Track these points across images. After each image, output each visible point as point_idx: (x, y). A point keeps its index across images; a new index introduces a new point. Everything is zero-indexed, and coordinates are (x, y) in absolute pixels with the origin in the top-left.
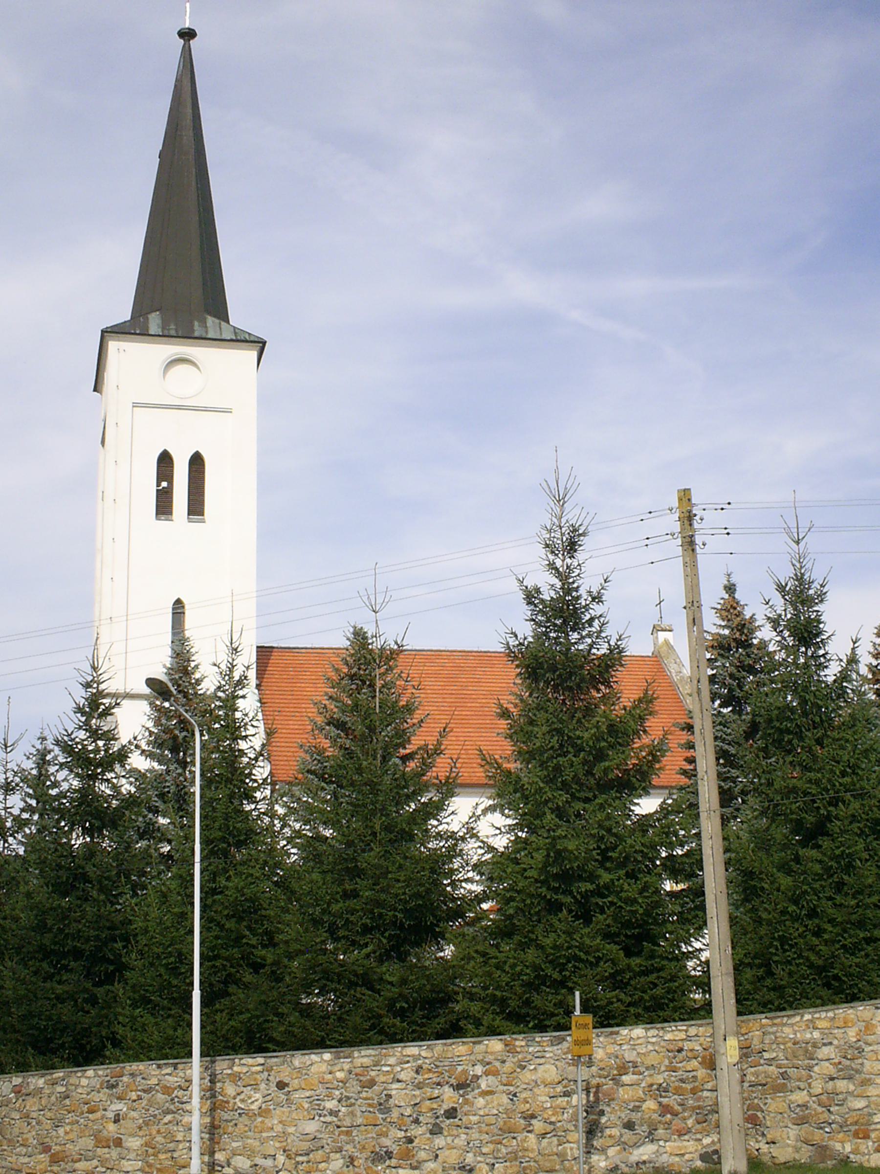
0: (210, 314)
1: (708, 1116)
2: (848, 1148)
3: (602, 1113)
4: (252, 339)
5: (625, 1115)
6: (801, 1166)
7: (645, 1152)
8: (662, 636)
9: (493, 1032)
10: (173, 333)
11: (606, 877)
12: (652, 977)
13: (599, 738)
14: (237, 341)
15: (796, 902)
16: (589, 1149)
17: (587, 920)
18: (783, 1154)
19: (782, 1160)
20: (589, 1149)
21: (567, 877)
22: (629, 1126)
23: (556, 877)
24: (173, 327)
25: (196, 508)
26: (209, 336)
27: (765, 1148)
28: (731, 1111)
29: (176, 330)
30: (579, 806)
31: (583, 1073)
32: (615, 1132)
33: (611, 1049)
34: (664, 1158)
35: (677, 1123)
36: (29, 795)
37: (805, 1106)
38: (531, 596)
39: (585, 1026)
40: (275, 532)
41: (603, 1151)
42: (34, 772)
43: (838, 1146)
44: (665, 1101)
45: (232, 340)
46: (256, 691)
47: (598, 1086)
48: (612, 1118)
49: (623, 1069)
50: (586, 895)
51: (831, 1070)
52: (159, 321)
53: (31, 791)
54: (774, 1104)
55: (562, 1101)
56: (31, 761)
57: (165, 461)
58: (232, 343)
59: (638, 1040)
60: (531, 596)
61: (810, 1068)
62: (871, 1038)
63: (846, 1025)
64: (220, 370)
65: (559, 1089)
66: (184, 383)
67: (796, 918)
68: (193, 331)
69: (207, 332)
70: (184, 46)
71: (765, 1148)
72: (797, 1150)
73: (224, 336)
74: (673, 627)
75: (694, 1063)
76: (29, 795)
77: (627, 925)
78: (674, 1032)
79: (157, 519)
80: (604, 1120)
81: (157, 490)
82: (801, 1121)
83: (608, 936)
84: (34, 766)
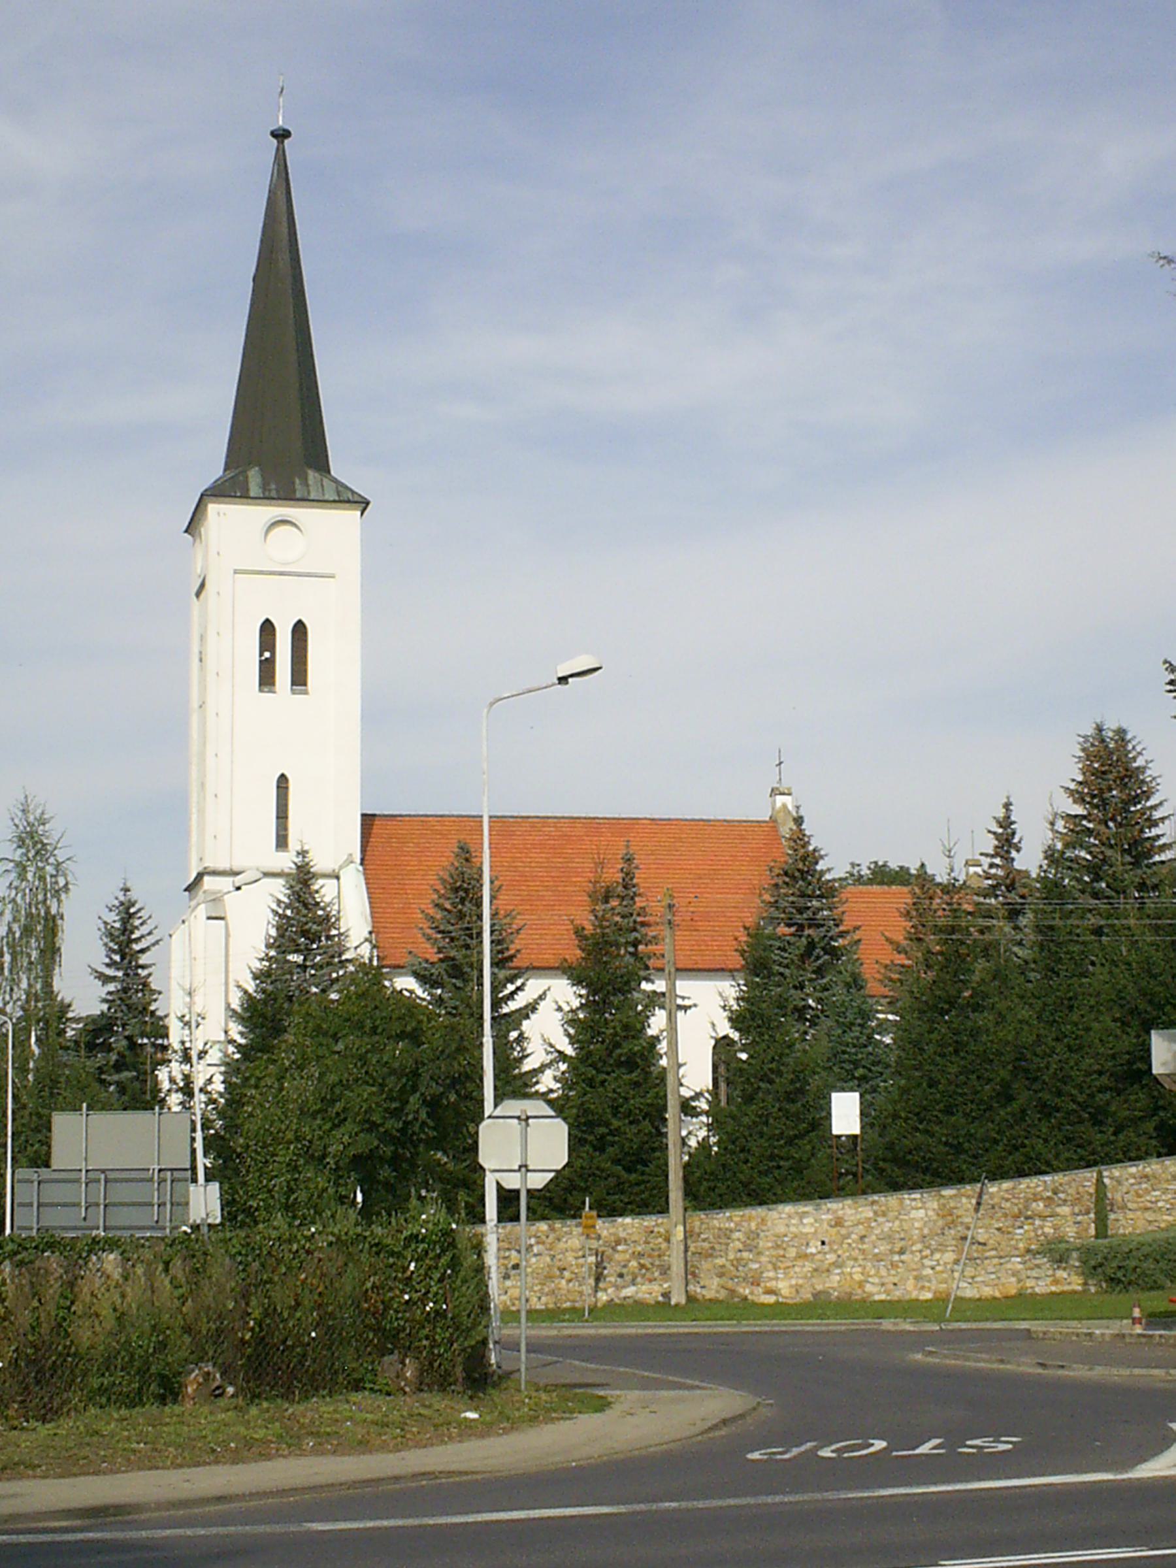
0: (310, 467)
1: (665, 1271)
2: (747, 1291)
3: (605, 1268)
4: (356, 498)
5: (618, 1270)
6: (721, 1302)
7: (629, 1291)
8: (780, 800)
9: (544, 1218)
10: (274, 494)
11: (616, 1123)
12: (642, 1187)
13: (616, 1034)
14: (340, 501)
15: (733, 1143)
16: (596, 1289)
17: (602, 1150)
18: (709, 1294)
19: (708, 1297)
20: (596, 1289)
21: (591, 1125)
22: (621, 1276)
23: (585, 1124)
24: (273, 486)
25: (299, 678)
26: (312, 497)
27: (699, 1290)
28: (677, 1267)
29: (277, 491)
30: (603, 1076)
31: (594, 1244)
32: (612, 1279)
33: (612, 1231)
34: (640, 1295)
35: (648, 1275)
36: (114, 951)
37: (723, 1266)
38: (579, 932)
39: (591, 1217)
40: (378, 715)
41: (605, 1290)
42: (117, 925)
43: (741, 1290)
44: (642, 1261)
45: (334, 501)
46: (361, 868)
47: (603, 1253)
48: (610, 1271)
49: (618, 1243)
50: (603, 1136)
51: (739, 1245)
52: (259, 480)
53: (116, 947)
54: (705, 1265)
55: (581, 1261)
56: (113, 914)
57: (267, 629)
58: (334, 505)
59: (628, 1224)
60: (579, 932)
61: (727, 1244)
62: (764, 1228)
63: (750, 1219)
64: (324, 532)
65: (580, 1253)
66: (286, 547)
67: (733, 1153)
68: (294, 491)
69: (309, 492)
70: (278, 149)
71: (699, 1290)
72: (717, 1292)
73: (327, 497)
74: (793, 791)
75: (660, 1240)
76: (114, 951)
77: (627, 1154)
78: (650, 1221)
79: (261, 691)
80: (606, 1272)
81: (261, 661)
82: (721, 1275)
83: (617, 1162)
84: (117, 918)
